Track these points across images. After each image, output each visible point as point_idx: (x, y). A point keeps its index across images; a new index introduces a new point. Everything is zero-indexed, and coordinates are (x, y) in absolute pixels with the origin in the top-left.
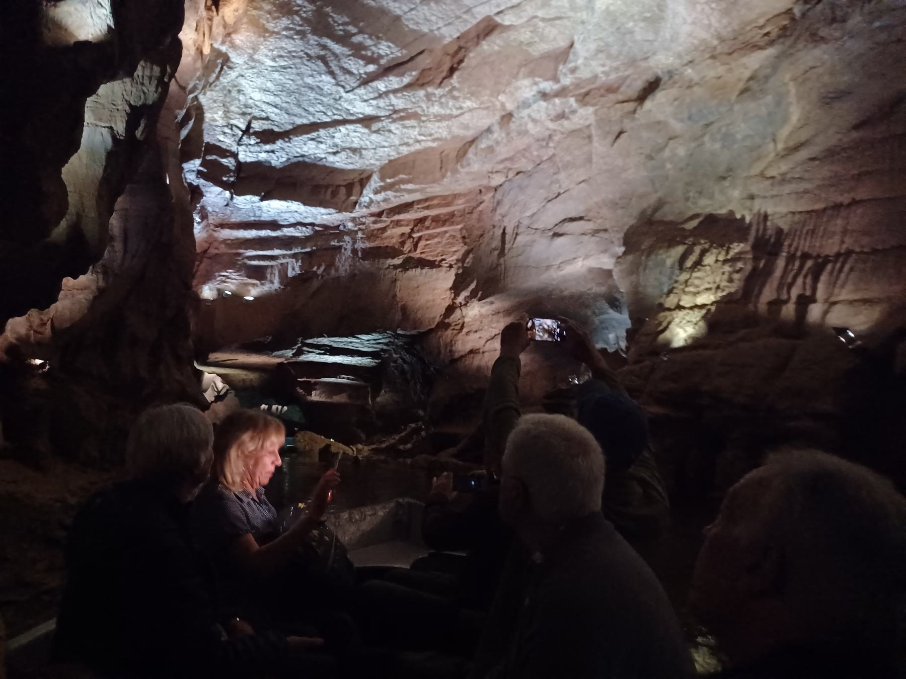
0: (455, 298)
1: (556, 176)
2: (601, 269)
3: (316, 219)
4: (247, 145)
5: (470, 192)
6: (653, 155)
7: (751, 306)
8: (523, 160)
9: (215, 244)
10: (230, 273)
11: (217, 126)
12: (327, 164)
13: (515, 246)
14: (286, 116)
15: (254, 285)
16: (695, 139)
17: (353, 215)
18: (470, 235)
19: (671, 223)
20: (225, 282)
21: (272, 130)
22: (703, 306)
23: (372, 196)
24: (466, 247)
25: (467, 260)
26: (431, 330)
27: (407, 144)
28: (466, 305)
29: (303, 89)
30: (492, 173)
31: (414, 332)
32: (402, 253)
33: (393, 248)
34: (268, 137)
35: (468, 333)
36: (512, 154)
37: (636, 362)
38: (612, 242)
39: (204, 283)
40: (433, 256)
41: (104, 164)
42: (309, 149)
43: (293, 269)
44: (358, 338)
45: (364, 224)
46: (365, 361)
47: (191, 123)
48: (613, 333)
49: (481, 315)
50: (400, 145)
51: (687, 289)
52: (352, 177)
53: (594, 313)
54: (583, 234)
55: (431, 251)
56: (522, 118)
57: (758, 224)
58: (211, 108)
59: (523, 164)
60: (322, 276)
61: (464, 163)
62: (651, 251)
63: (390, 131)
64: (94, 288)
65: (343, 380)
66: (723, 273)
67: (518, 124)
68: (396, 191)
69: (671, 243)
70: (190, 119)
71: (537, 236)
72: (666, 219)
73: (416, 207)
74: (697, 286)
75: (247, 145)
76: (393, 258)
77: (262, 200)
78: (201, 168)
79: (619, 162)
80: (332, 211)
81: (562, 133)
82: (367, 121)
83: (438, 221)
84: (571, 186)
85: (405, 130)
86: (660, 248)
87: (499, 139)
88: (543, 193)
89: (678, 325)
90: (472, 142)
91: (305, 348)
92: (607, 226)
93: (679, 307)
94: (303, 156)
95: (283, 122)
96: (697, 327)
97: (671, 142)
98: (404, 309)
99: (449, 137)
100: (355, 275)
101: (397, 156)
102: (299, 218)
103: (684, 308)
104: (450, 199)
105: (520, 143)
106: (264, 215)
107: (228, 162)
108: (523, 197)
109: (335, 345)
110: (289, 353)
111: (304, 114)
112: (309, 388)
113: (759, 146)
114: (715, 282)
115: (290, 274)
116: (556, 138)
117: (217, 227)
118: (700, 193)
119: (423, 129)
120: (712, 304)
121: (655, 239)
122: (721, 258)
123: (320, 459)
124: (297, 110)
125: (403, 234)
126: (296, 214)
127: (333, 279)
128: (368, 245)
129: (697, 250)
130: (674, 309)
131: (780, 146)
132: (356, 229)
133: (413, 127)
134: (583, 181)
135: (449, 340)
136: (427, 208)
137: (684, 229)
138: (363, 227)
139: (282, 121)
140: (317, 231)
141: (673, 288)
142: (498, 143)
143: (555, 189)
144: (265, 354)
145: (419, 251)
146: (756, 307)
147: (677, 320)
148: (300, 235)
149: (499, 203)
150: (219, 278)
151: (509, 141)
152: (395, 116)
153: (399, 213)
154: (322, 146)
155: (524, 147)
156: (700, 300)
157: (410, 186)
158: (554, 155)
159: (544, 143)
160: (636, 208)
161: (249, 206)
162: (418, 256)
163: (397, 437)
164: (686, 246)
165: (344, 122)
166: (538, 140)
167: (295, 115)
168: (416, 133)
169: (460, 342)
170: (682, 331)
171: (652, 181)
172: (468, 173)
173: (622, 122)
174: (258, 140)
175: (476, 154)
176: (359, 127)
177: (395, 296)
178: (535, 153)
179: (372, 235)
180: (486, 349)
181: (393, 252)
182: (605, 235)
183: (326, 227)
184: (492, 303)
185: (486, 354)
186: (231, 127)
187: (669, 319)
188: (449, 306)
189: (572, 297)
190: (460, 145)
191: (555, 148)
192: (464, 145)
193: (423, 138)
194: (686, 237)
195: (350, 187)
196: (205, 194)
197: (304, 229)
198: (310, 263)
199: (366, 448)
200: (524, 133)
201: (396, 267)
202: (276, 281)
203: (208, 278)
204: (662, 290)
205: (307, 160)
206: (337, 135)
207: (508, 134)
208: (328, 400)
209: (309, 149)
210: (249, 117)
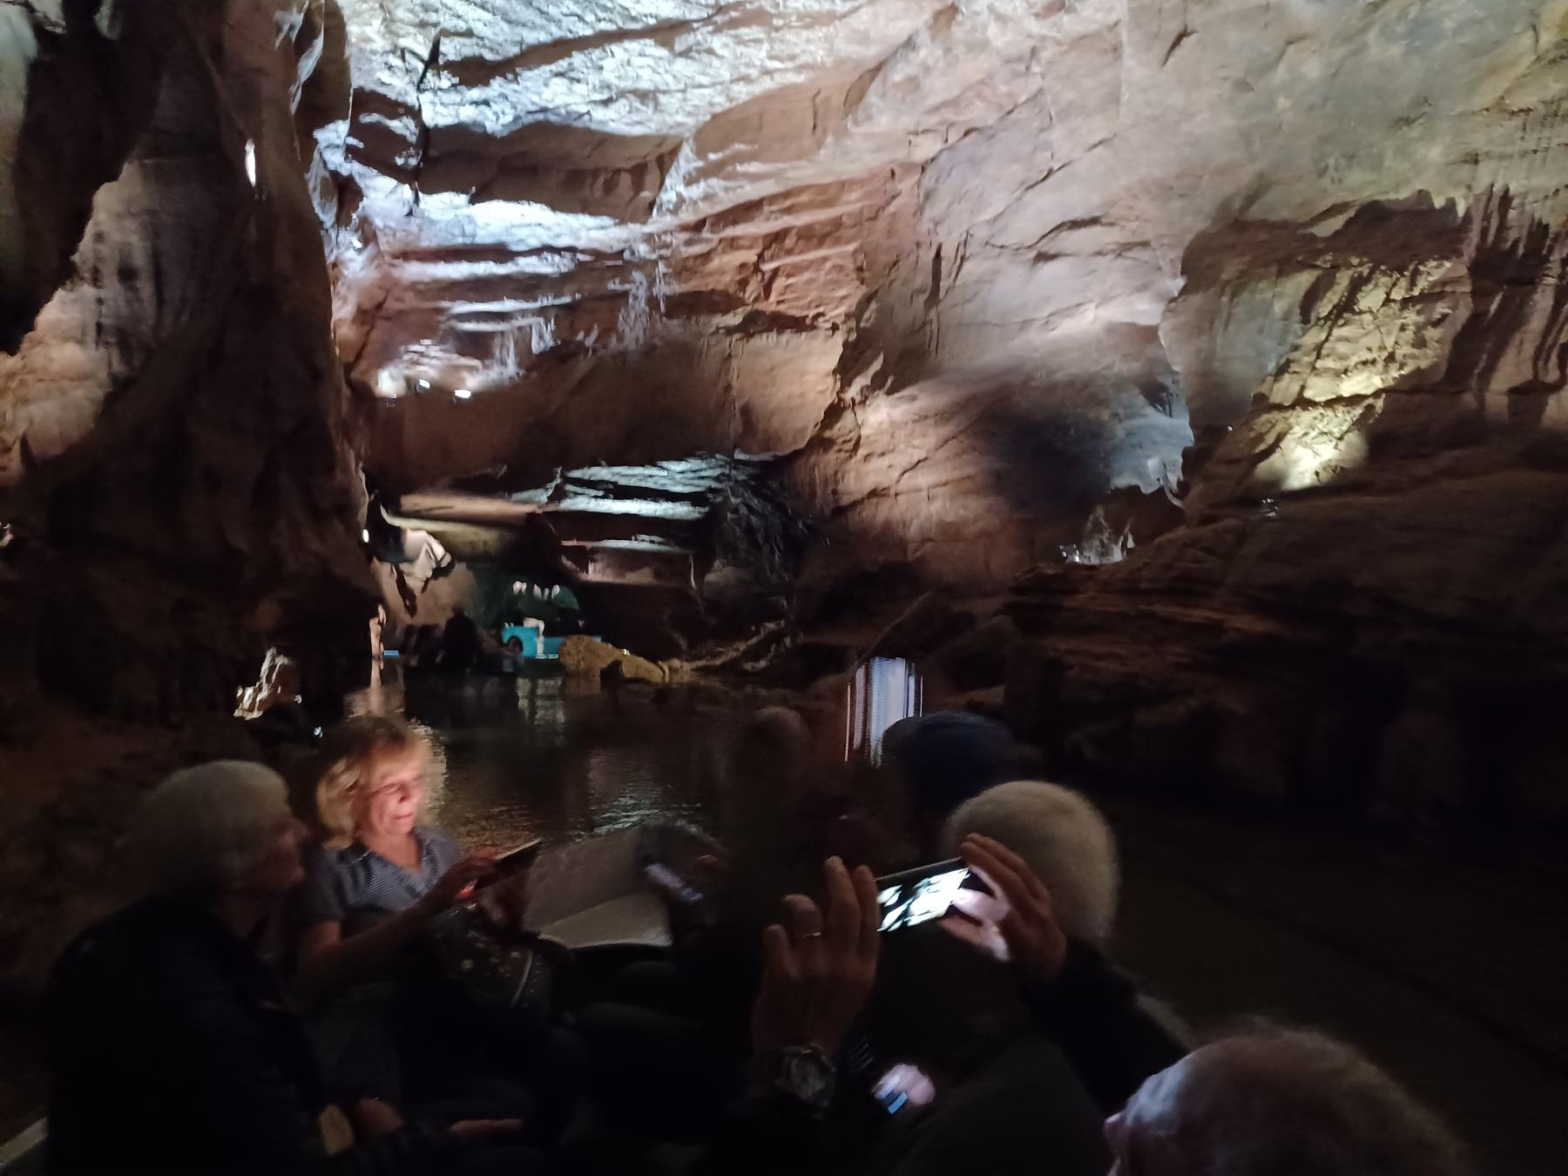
0: (842, 390)
1: (1043, 136)
2: (1133, 325)
3: (578, 238)
4: (435, 91)
5: (873, 176)
6: (1249, 80)
7: (1469, 399)
8: (979, 104)
9: (397, 292)
10: (425, 345)
11: (374, 52)
12: (593, 126)
13: (958, 282)
14: (506, 27)
15: (471, 369)
16: (1347, 39)
17: (648, 229)
18: (871, 264)
19: (1284, 225)
20: (417, 363)
21: (481, 58)
22: (1355, 400)
23: (681, 188)
24: (864, 290)
25: (866, 316)
26: (797, 454)
27: (746, 79)
28: (863, 402)
30: (917, 134)
31: (766, 457)
32: (744, 304)
33: (725, 293)
34: (473, 72)
35: (867, 458)
36: (956, 92)
37: (1207, 520)
38: (1159, 268)
39: (380, 365)
40: (801, 308)
41: (24, 92)
42: (555, 94)
43: (541, 337)
45: (667, 246)
46: (681, 510)
47: (319, 43)
48: (1155, 454)
49: (892, 422)
50: (732, 82)
51: (1319, 364)
52: (643, 152)
53: (1116, 415)
54: (1099, 253)
55: (797, 299)
56: (977, 14)
57: (1487, 218)
58: (358, 14)
59: (978, 113)
60: (594, 351)
61: (860, 114)
62: (1239, 286)
63: (710, 52)
64: (103, 375)
65: (643, 543)
66: (1403, 328)
67: (967, 27)
68: (727, 178)
69: (1286, 266)
70: (316, 36)
71: (1003, 262)
72: (1273, 217)
73: (766, 209)
74: (1343, 358)
75: (435, 91)
76: (725, 312)
77: (473, 201)
78: (352, 141)
79: (1177, 99)
80: (606, 221)
81: (1059, 43)
83: (812, 237)
84: (1076, 155)
85: (741, 49)
86: (1261, 278)
87: (930, 62)
88: (1016, 172)
89: (1299, 441)
90: (878, 68)
91: (569, 487)
92: (1149, 236)
93: (1303, 403)
94: (544, 110)
95: (501, 39)
96: (1342, 445)
97: (1292, 48)
98: (746, 411)
99: (829, 61)
100: (654, 347)
101: (728, 105)
102: (545, 238)
103: (1314, 404)
104: (832, 191)
105: (972, 68)
108: (977, 182)
109: (623, 482)
110: (542, 496)
111: (539, 21)
112: (583, 558)
113: (1497, 43)
114: (1382, 348)
115: (536, 346)
116: (1045, 55)
117: (396, 257)
118: (1351, 158)
119: (776, 46)
120: (1377, 394)
121: (1247, 258)
122: (1397, 295)
123: (603, 685)
125: (743, 266)
126: (539, 230)
127: (614, 357)
128: (677, 288)
129: (1343, 279)
130: (1292, 407)
131: (1547, 38)
132: (654, 256)
133: (758, 41)
134: (1100, 143)
135: (830, 472)
136: (789, 211)
137: (1313, 238)
138: (663, 252)
139: (496, 36)
140: (580, 264)
141: (1289, 362)
142: (927, 70)
143: (1043, 161)
144: (502, 497)
145: (773, 298)
146: (1481, 401)
147: (1298, 431)
149: (928, 196)
150: (406, 357)
151: (949, 65)
152: (719, 19)
153: (735, 222)
155: (981, 76)
156: (1348, 388)
157: (754, 167)
158: (1041, 91)
159: (1022, 68)
160: (1213, 193)
161: (450, 216)
163: (742, 646)
164: (1316, 273)
165: (620, 36)
166: (1008, 61)
167: (524, 25)
168: (763, 54)
169: (852, 474)
170: (1310, 453)
171: (1246, 136)
172: (867, 136)
173: (1185, 10)
174: (456, 80)
175: (883, 96)
176: (648, 45)
177: (728, 387)
178: (1003, 89)
179: (685, 269)
180: (903, 486)
182: (1144, 255)
183: (598, 255)
184: (913, 398)
185: (900, 498)
186: (402, 53)
187: (1279, 428)
188: (832, 406)
189: (1070, 383)
190: (850, 78)
191: (1043, 76)
192: (861, 77)
194: (1320, 253)
195: (639, 172)
196: (365, 191)
197: (557, 258)
198: (572, 324)
199: (687, 666)
200: (979, 46)
201: (730, 331)
202: (511, 361)
203: (386, 356)
204: (1263, 367)
205: (552, 118)
206: (608, 64)
207: (948, 50)
208: (618, 581)
209: (555, 94)
210: (433, 32)
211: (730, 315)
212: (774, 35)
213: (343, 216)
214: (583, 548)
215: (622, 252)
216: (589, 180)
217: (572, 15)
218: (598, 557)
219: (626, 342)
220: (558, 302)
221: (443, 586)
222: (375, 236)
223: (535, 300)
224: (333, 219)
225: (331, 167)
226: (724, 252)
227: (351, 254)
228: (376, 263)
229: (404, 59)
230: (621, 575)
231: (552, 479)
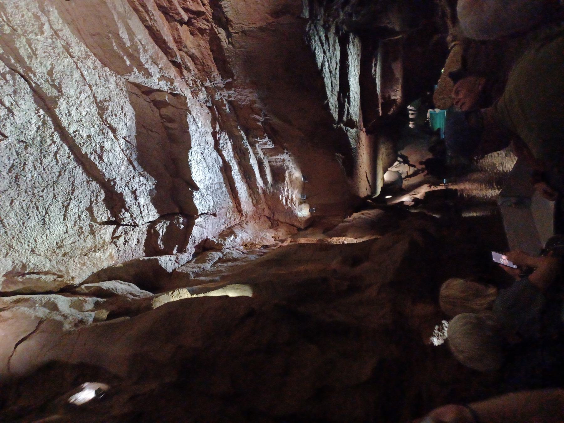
3: (206, 132)
15: (290, 175)
17: (189, 95)
20: (292, 200)
21: (104, 200)
23: (155, 79)
27: (67, 47)
29: (23, 187)
32: (212, 29)
33: (211, 43)
34: (115, 202)
39: (296, 216)
43: (265, 144)
44: (323, 65)
47: (106, 285)
60: (266, 115)
63: (50, 73)
65: (377, 71)
68: (138, 51)
76: (219, 40)
77: (197, 189)
80: (189, 119)
82: (46, 103)
91: (345, 118)
94: (130, 162)
98: (276, 14)
101: (93, 57)
106: (216, 180)
107: (162, 229)
109: (337, 89)
110: (352, 132)
112: (388, 103)
115: (271, 146)
124: (64, 183)
125: (192, 33)
126: (206, 152)
127: (265, 105)
128: (215, 73)
132: (203, 89)
145: (202, 9)
148: (229, 144)
150: (290, 205)
153: (164, 42)
154: (107, 145)
162: (208, 8)
177: (261, 29)
181: (214, 41)
193: (46, 27)
196: (204, 238)
197: (221, 141)
201: (229, 35)
203: (290, 213)
205: (134, 156)
208: (400, 81)
210: (96, 226)
211: (220, 36)
212: (19, 31)
213: (217, 248)
214: (382, 104)
215: (209, 107)
216: (170, 131)
217: (56, 158)
218: (387, 95)
219: (254, 98)
220: (245, 138)
221: (413, 159)
222: (229, 228)
223: (247, 149)
224: (218, 253)
225: (191, 257)
226: (185, 47)
227: (238, 240)
228: (244, 225)
229: (120, 236)
230: (397, 80)
231: (341, 129)
